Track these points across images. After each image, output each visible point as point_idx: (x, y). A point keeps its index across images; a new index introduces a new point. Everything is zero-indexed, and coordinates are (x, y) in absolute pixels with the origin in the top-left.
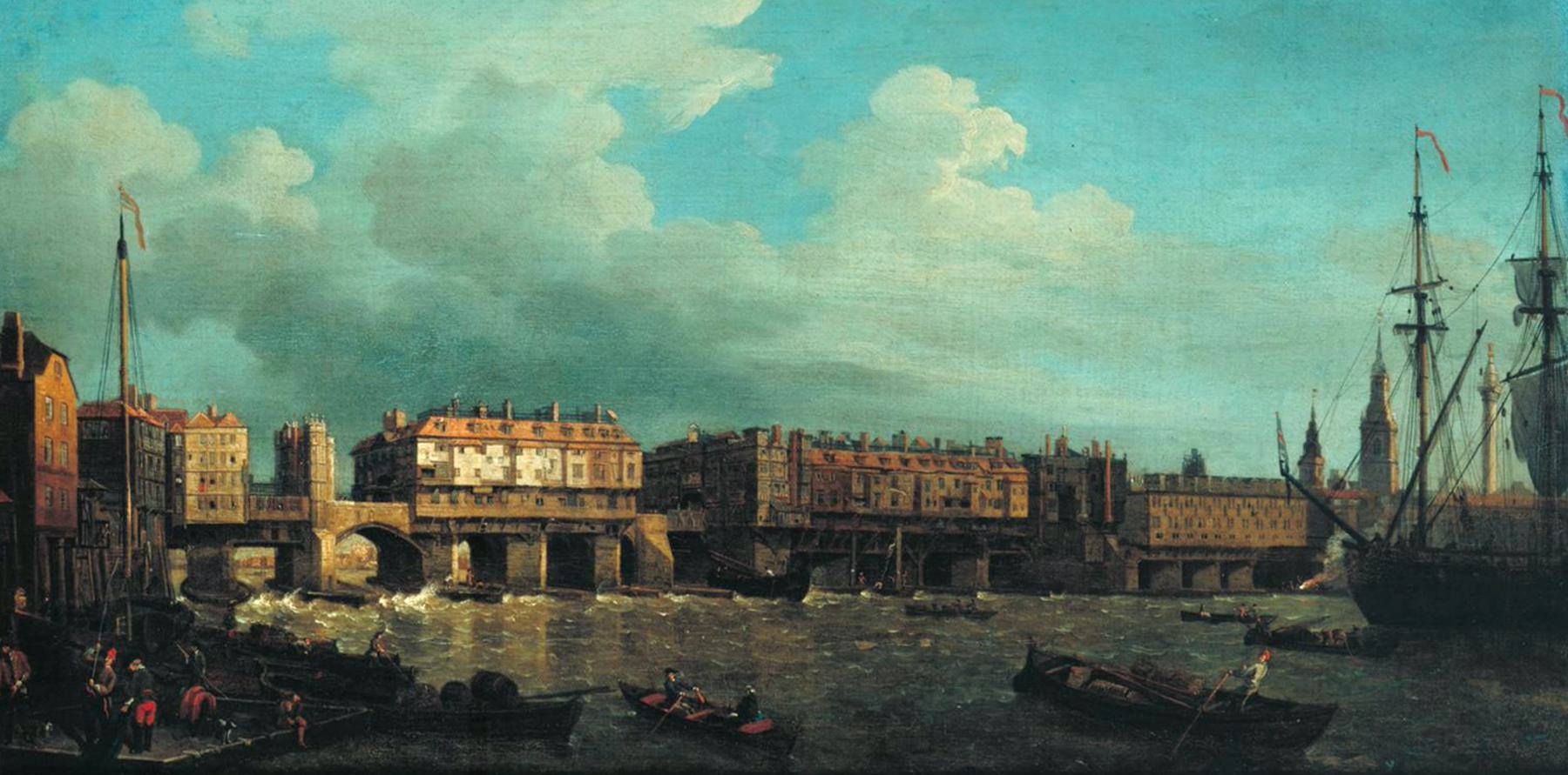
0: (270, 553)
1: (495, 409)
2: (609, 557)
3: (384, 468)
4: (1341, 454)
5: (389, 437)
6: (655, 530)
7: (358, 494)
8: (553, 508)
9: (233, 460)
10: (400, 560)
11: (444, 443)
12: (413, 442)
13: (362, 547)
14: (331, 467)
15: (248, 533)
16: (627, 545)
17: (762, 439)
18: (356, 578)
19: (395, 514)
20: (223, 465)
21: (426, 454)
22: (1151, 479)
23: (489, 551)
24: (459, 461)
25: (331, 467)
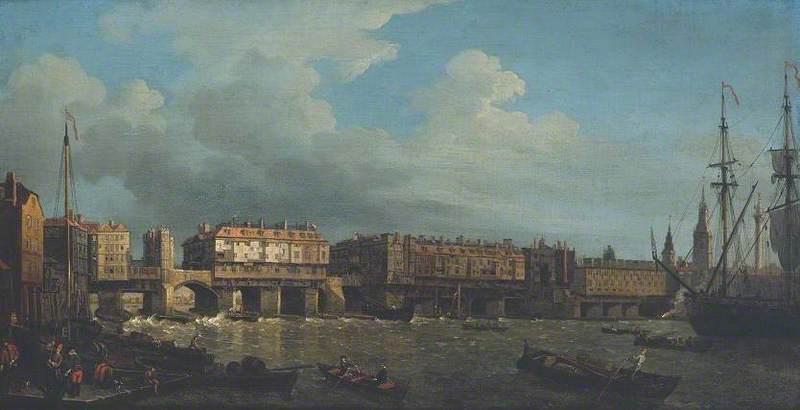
0: (140, 296)
1: (256, 220)
2: (313, 299)
3: (198, 253)
4: (683, 249)
5: (201, 237)
6: (336, 285)
7: (186, 266)
8: (284, 274)
9: (122, 248)
10: (207, 300)
11: (229, 240)
12: (214, 240)
13: (187, 293)
14: (171, 252)
15: (129, 286)
16: (321, 292)
17: (390, 239)
18: (184, 309)
19: (204, 276)
20: (117, 250)
21: (220, 246)
22: (587, 261)
23: (251, 295)
24: (236, 249)
25: (171, 252)
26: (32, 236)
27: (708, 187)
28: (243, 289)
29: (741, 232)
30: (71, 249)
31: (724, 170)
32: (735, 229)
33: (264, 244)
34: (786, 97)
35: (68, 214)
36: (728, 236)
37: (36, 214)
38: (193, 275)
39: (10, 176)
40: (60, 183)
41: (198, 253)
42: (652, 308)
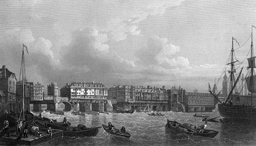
6: (110, 103)
10: (68, 107)
22: (189, 93)
25: (57, 92)
26: (13, 89)
27: (227, 73)
28: (79, 103)
29: (237, 84)
30: (25, 89)
31: (232, 65)
32: (235, 84)
33: (86, 90)
34: (232, 64)
35: (24, 79)
36: (233, 85)
37: (13, 81)
38: (63, 99)
39: (4, 66)
40: (20, 75)
41: (66, 92)
42: (209, 109)
